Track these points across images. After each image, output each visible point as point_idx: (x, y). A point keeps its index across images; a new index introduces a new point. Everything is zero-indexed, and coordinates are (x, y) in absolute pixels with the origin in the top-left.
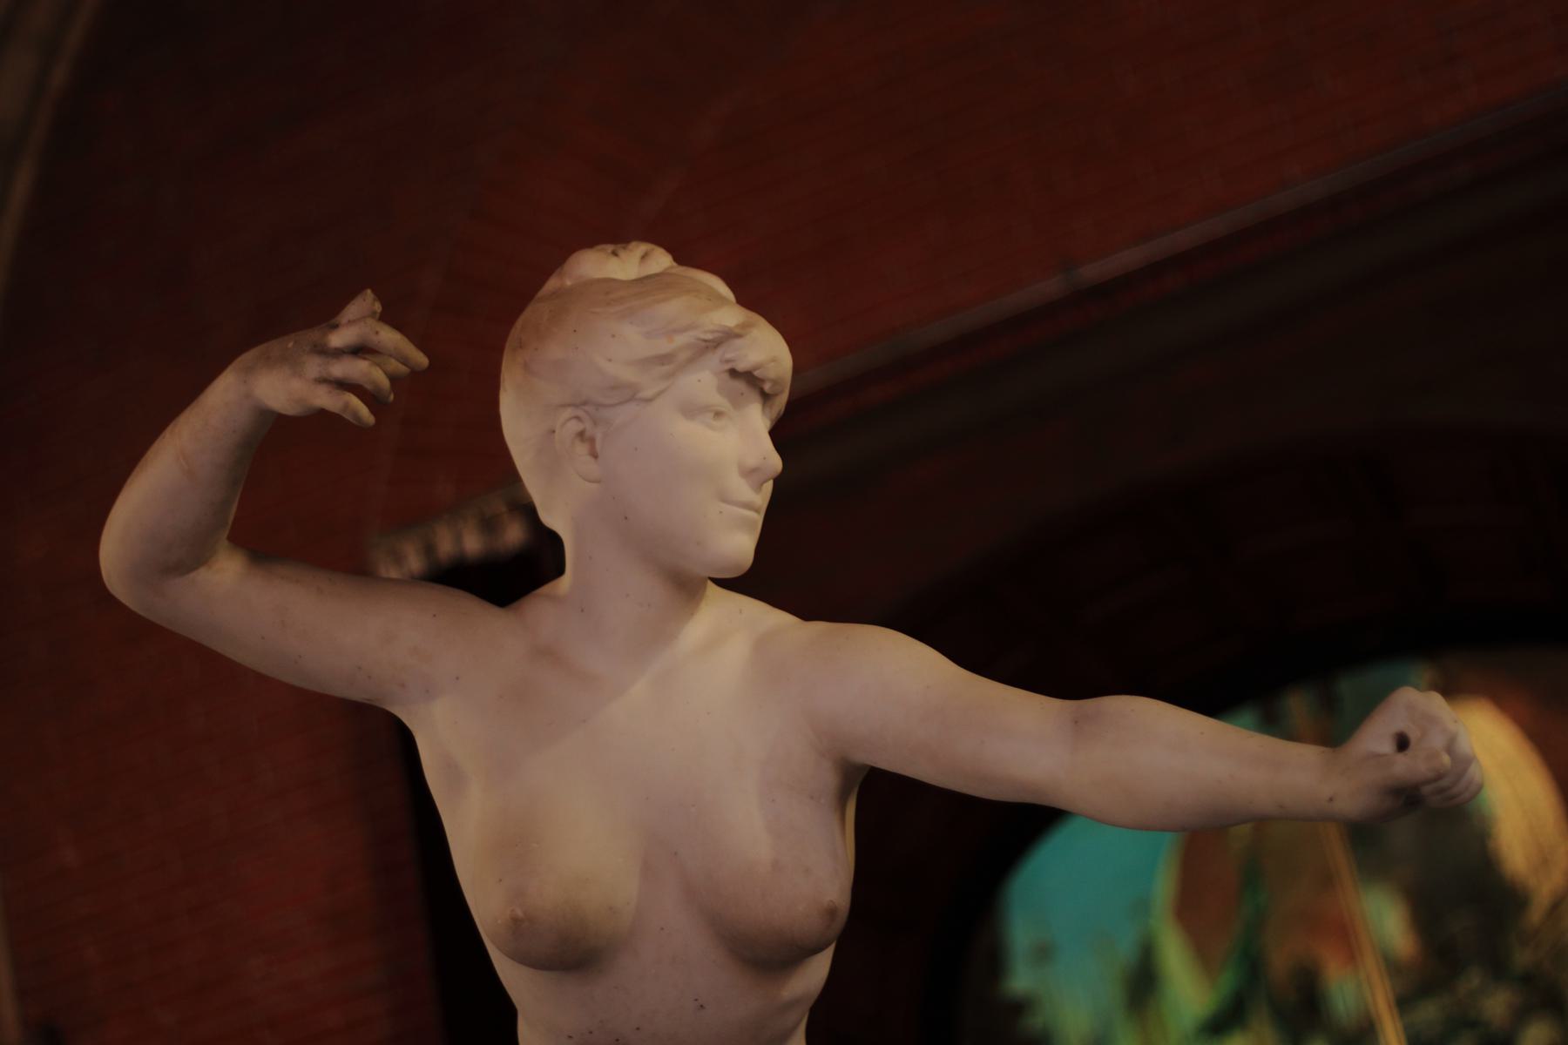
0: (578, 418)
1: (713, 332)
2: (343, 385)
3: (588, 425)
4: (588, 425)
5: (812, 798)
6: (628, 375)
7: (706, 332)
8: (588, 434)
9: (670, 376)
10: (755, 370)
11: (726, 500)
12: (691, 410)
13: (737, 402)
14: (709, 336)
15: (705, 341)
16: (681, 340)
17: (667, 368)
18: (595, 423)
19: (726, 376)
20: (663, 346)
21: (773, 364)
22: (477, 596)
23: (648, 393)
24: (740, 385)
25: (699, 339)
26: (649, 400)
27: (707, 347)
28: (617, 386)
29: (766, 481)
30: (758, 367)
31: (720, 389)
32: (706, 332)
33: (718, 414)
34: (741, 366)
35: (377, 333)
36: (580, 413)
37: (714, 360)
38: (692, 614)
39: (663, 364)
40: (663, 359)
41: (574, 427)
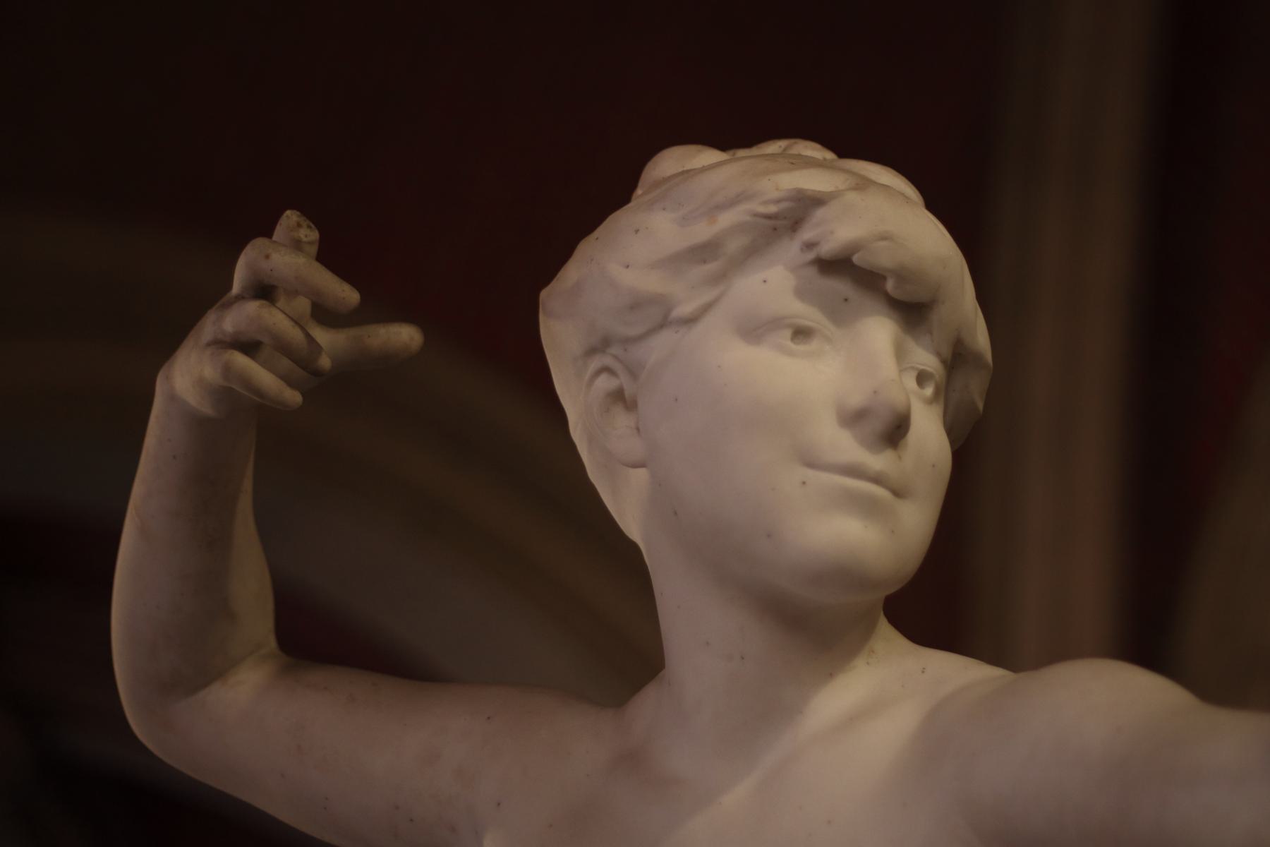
0: (606, 369)
1: (778, 201)
2: (877, 479)
3: (624, 380)
4: (624, 380)
6: (651, 283)
7: (766, 203)
8: (627, 394)
9: (721, 278)
10: (853, 254)
11: (812, 463)
13: (840, 314)
14: (772, 209)
16: (726, 219)
17: (712, 267)
18: (633, 374)
19: (812, 272)
20: (702, 232)
23: (685, 309)
24: (840, 286)
25: (756, 215)
26: (691, 321)
28: (638, 303)
29: (275, 242)
30: (855, 247)
31: (801, 293)
32: (766, 203)
33: (802, 333)
34: (828, 248)
35: (267, 257)
36: (607, 360)
37: (791, 250)
38: (831, 675)
39: (705, 262)
40: (704, 252)
41: (605, 384)
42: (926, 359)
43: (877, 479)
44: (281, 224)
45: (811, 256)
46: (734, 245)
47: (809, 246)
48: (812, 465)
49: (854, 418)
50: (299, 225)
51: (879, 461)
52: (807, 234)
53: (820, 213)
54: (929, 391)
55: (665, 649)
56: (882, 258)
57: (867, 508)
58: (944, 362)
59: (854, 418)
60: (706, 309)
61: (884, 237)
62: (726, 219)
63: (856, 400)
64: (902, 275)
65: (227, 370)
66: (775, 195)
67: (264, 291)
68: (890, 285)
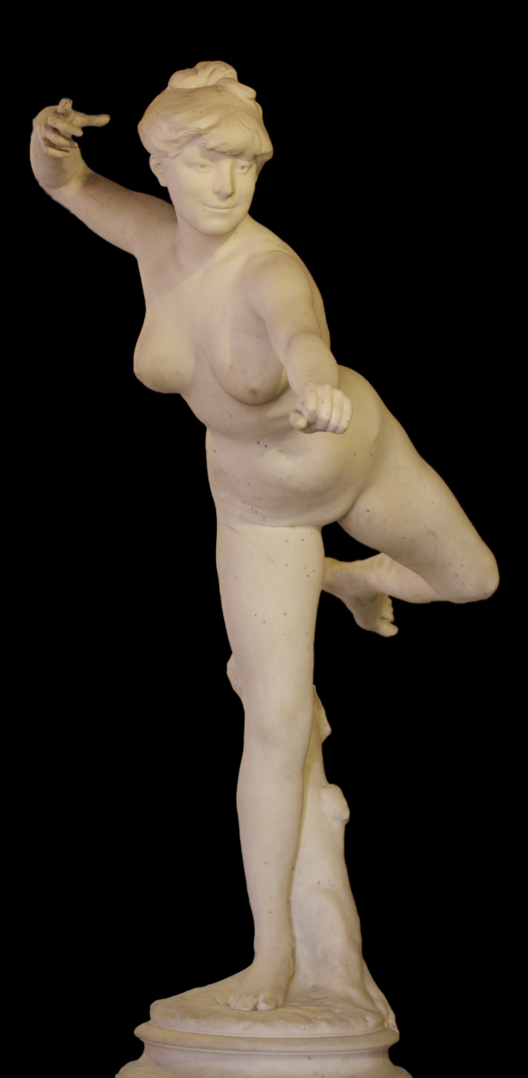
1: (194, 131)
6: (162, 147)
7: (190, 131)
9: (180, 148)
12: (190, 164)
13: (213, 159)
14: (193, 133)
15: (192, 135)
16: (181, 134)
17: (178, 145)
20: (174, 136)
23: (172, 155)
24: (212, 153)
26: (174, 157)
27: (194, 137)
31: (202, 156)
32: (190, 131)
33: (202, 166)
37: (199, 142)
40: (176, 141)
44: (62, 103)
47: (203, 144)
48: (206, 205)
50: (66, 103)
53: (205, 136)
55: (131, 191)
56: (224, 149)
57: (223, 216)
59: (217, 193)
63: (217, 189)
64: (230, 152)
68: (228, 153)
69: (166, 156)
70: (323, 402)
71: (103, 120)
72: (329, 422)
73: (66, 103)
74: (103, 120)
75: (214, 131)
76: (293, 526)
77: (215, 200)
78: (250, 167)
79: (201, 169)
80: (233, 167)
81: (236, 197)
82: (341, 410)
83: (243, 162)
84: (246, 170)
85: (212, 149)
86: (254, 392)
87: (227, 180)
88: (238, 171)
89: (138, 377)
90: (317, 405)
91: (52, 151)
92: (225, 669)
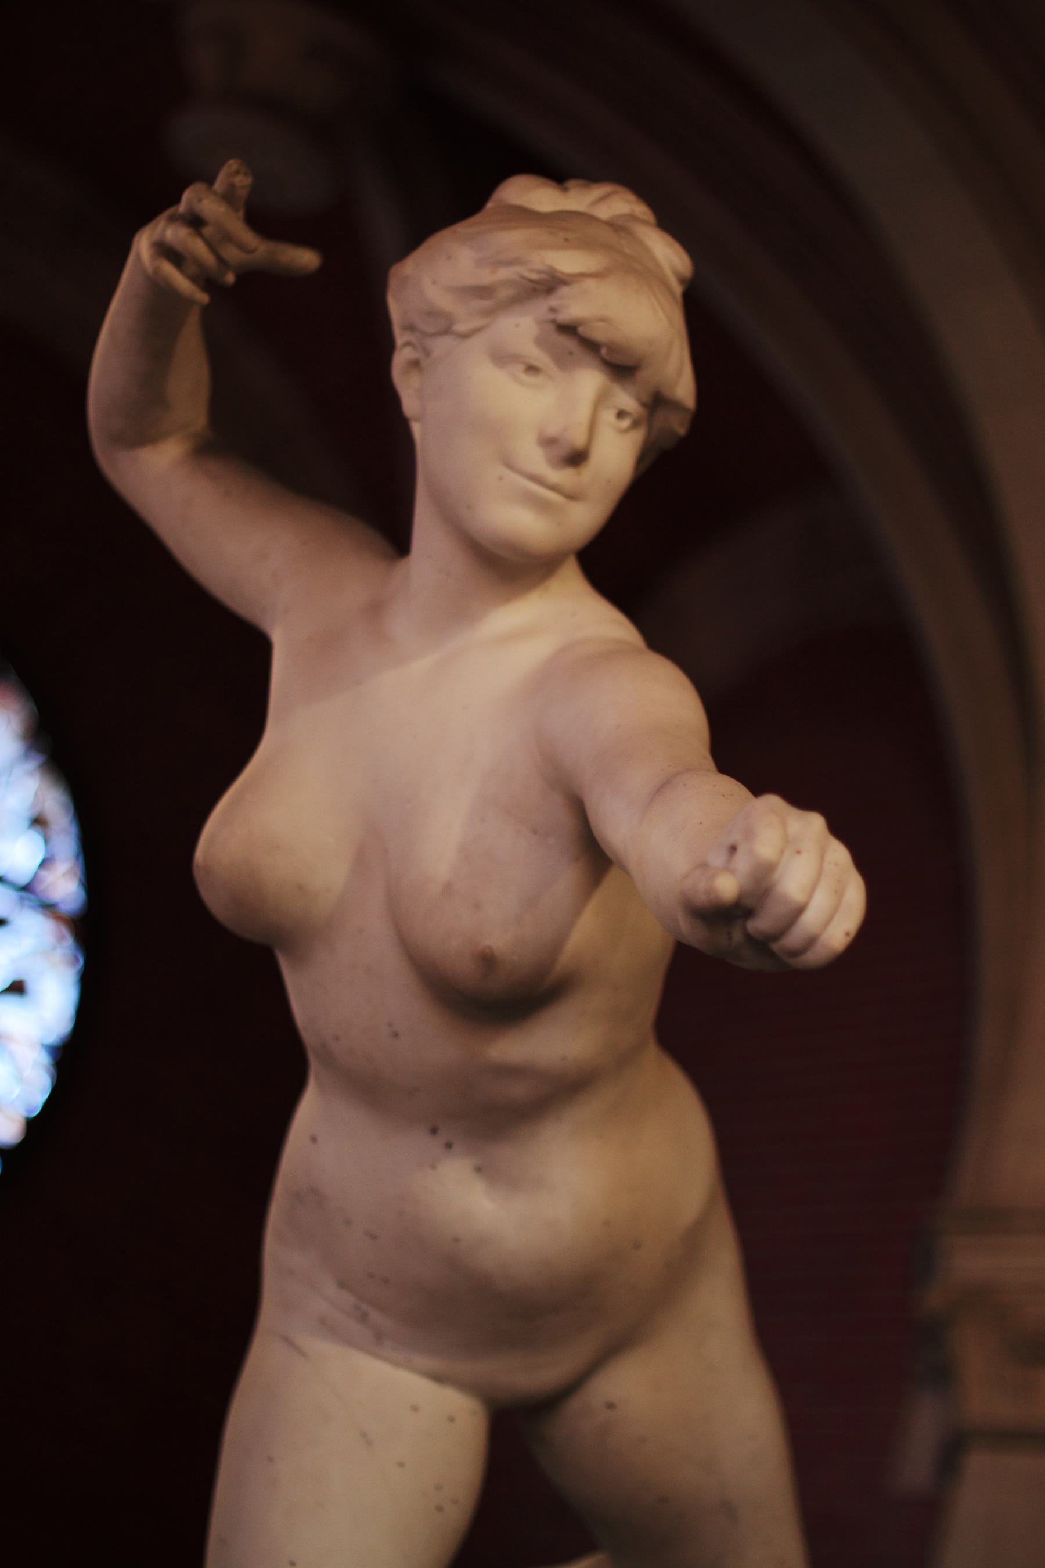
1: (539, 272)
2: (554, 488)
5: (535, 832)
6: (444, 301)
7: (532, 271)
9: (490, 313)
11: (509, 465)
12: (502, 358)
13: (564, 362)
14: (534, 276)
15: (531, 281)
16: (504, 273)
17: (485, 304)
19: (551, 328)
20: (486, 277)
21: (600, 324)
22: (685, 945)
23: (461, 327)
24: (568, 343)
25: (523, 277)
26: (465, 336)
27: (534, 290)
28: (433, 313)
30: (581, 322)
31: (540, 342)
32: (532, 271)
33: (532, 369)
34: (563, 317)
35: (200, 200)
37: (541, 307)
40: (483, 292)
42: (626, 399)
43: (554, 488)
45: (552, 316)
46: (504, 293)
47: (553, 310)
49: (548, 442)
50: (237, 172)
51: (563, 477)
52: (553, 301)
53: (564, 290)
54: (626, 423)
56: (599, 333)
57: (543, 506)
58: (644, 405)
59: (548, 442)
60: (477, 331)
61: (602, 320)
62: (504, 273)
63: (552, 431)
64: (612, 348)
65: (157, 271)
66: (538, 266)
67: (195, 222)
68: (603, 351)
69: (447, 331)
70: (799, 852)
71: (307, 259)
72: (799, 910)
73: (237, 172)
74: (307, 259)
75: (590, 284)
76: (438, 1378)
77: (537, 460)
78: (635, 424)
79: (524, 377)
80: (601, 400)
81: (588, 473)
82: (839, 894)
83: (626, 399)
84: (626, 423)
85: (568, 329)
86: (488, 960)
87: (583, 414)
88: (608, 416)
89: (199, 875)
90: (782, 852)
91: (168, 268)
92: (862, 862)
